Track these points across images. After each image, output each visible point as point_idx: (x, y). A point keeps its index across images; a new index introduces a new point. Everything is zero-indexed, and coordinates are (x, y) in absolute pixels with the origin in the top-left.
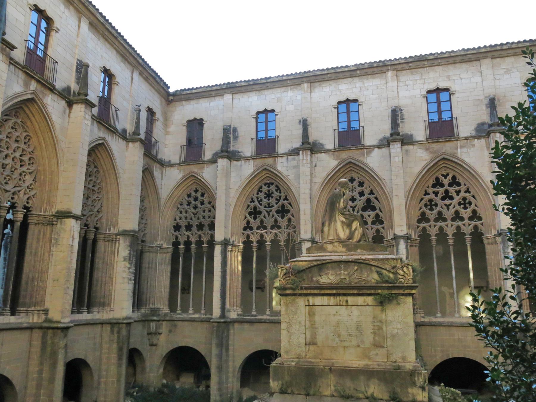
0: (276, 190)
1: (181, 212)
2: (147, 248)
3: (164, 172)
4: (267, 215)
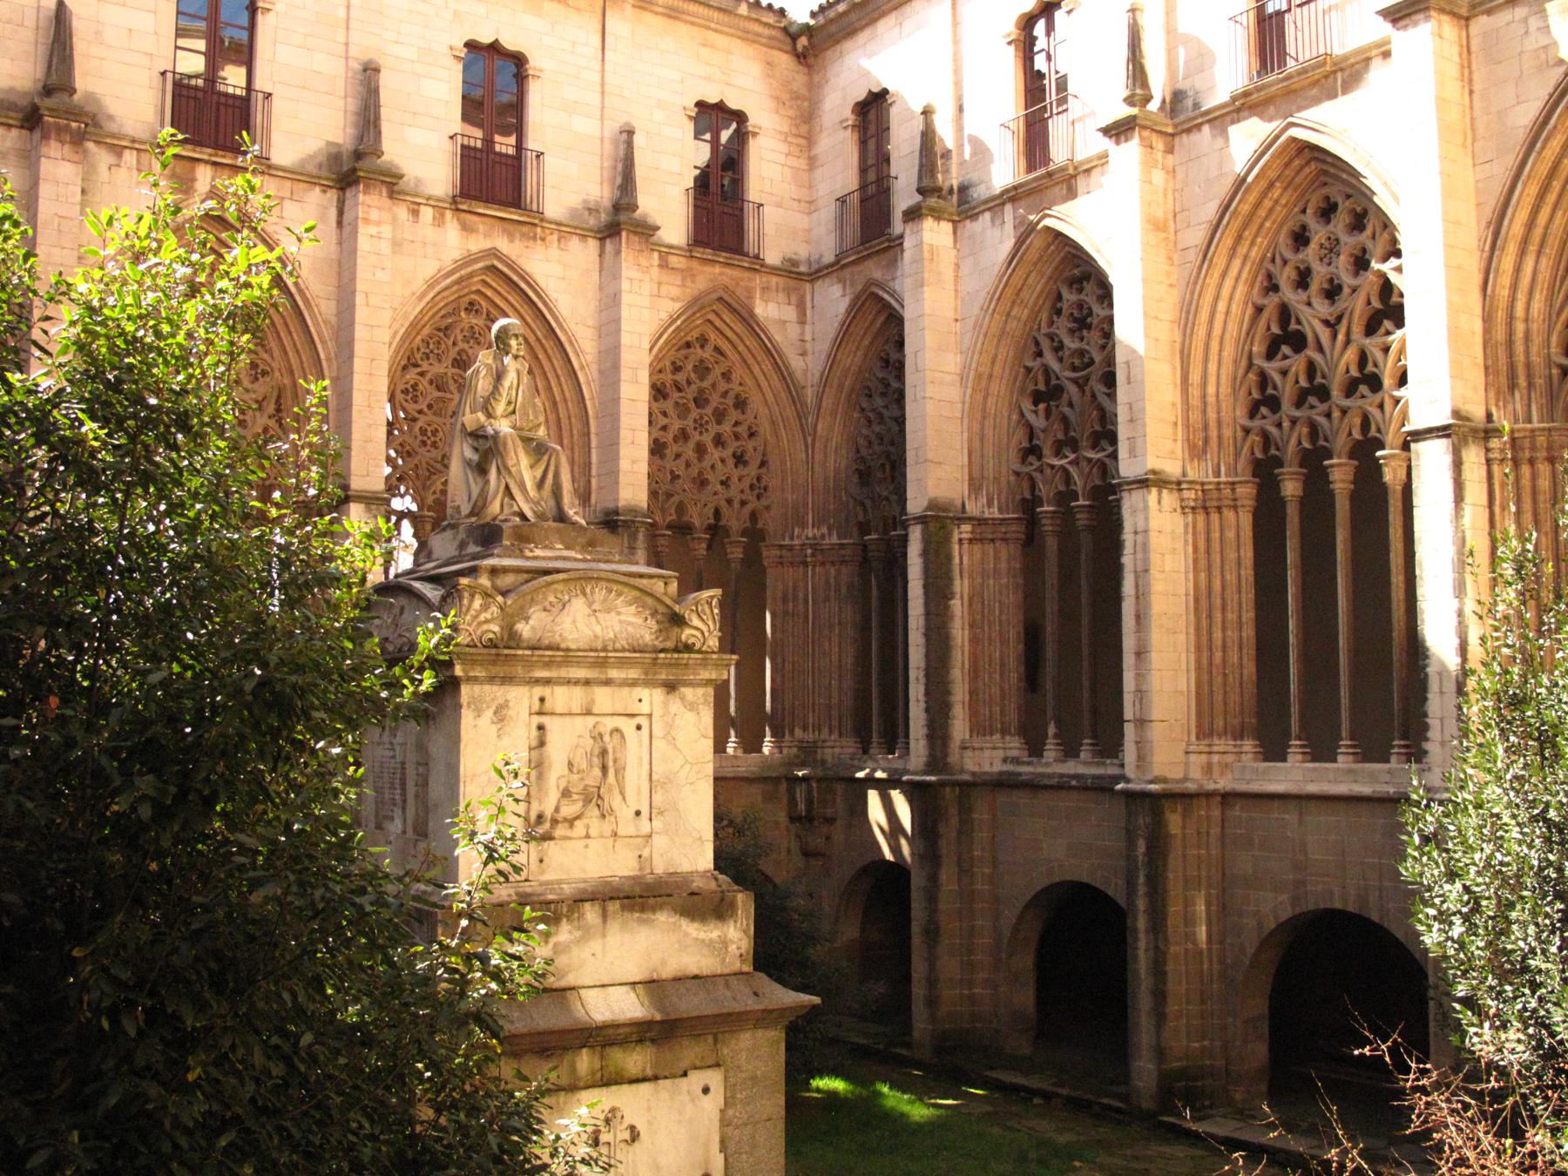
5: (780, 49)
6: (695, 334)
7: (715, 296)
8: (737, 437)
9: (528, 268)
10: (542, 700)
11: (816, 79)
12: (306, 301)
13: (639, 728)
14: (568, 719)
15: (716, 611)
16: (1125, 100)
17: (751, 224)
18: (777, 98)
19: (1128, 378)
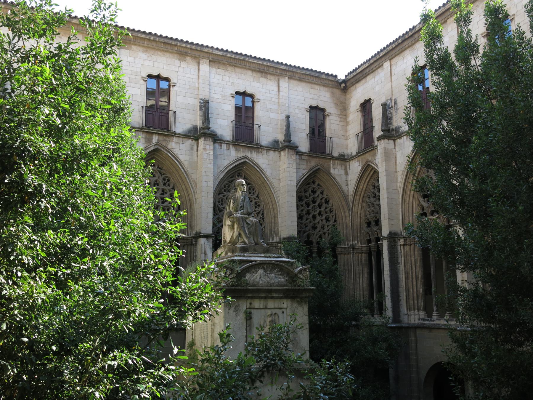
2: (340, 250)
3: (348, 167)
9: (257, 162)
10: (251, 304)
11: (348, 96)
12: (187, 174)
13: (283, 312)
14: (259, 310)
17: (171, 119)
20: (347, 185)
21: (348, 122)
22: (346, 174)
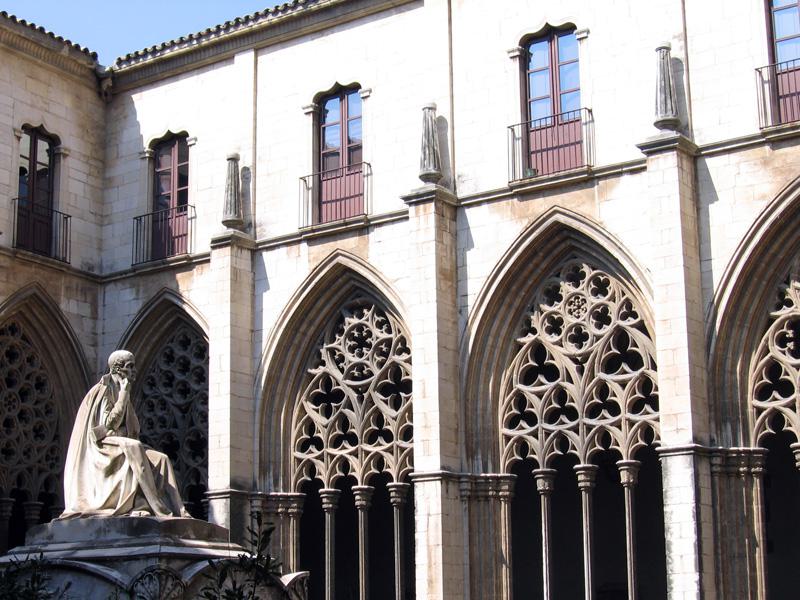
0: (342, 358)
1: (151, 407)
3: (100, 297)
4: (574, 374)
5: (86, 86)
6: (9, 323)
7: (29, 293)
8: (38, 414)
11: (114, 113)
15: (306, 588)
16: (420, 177)
17: (59, 232)
18: (82, 126)
19: (424, 392)
20: (95, 345)
21: (110, 180)
22: (94, 317)
